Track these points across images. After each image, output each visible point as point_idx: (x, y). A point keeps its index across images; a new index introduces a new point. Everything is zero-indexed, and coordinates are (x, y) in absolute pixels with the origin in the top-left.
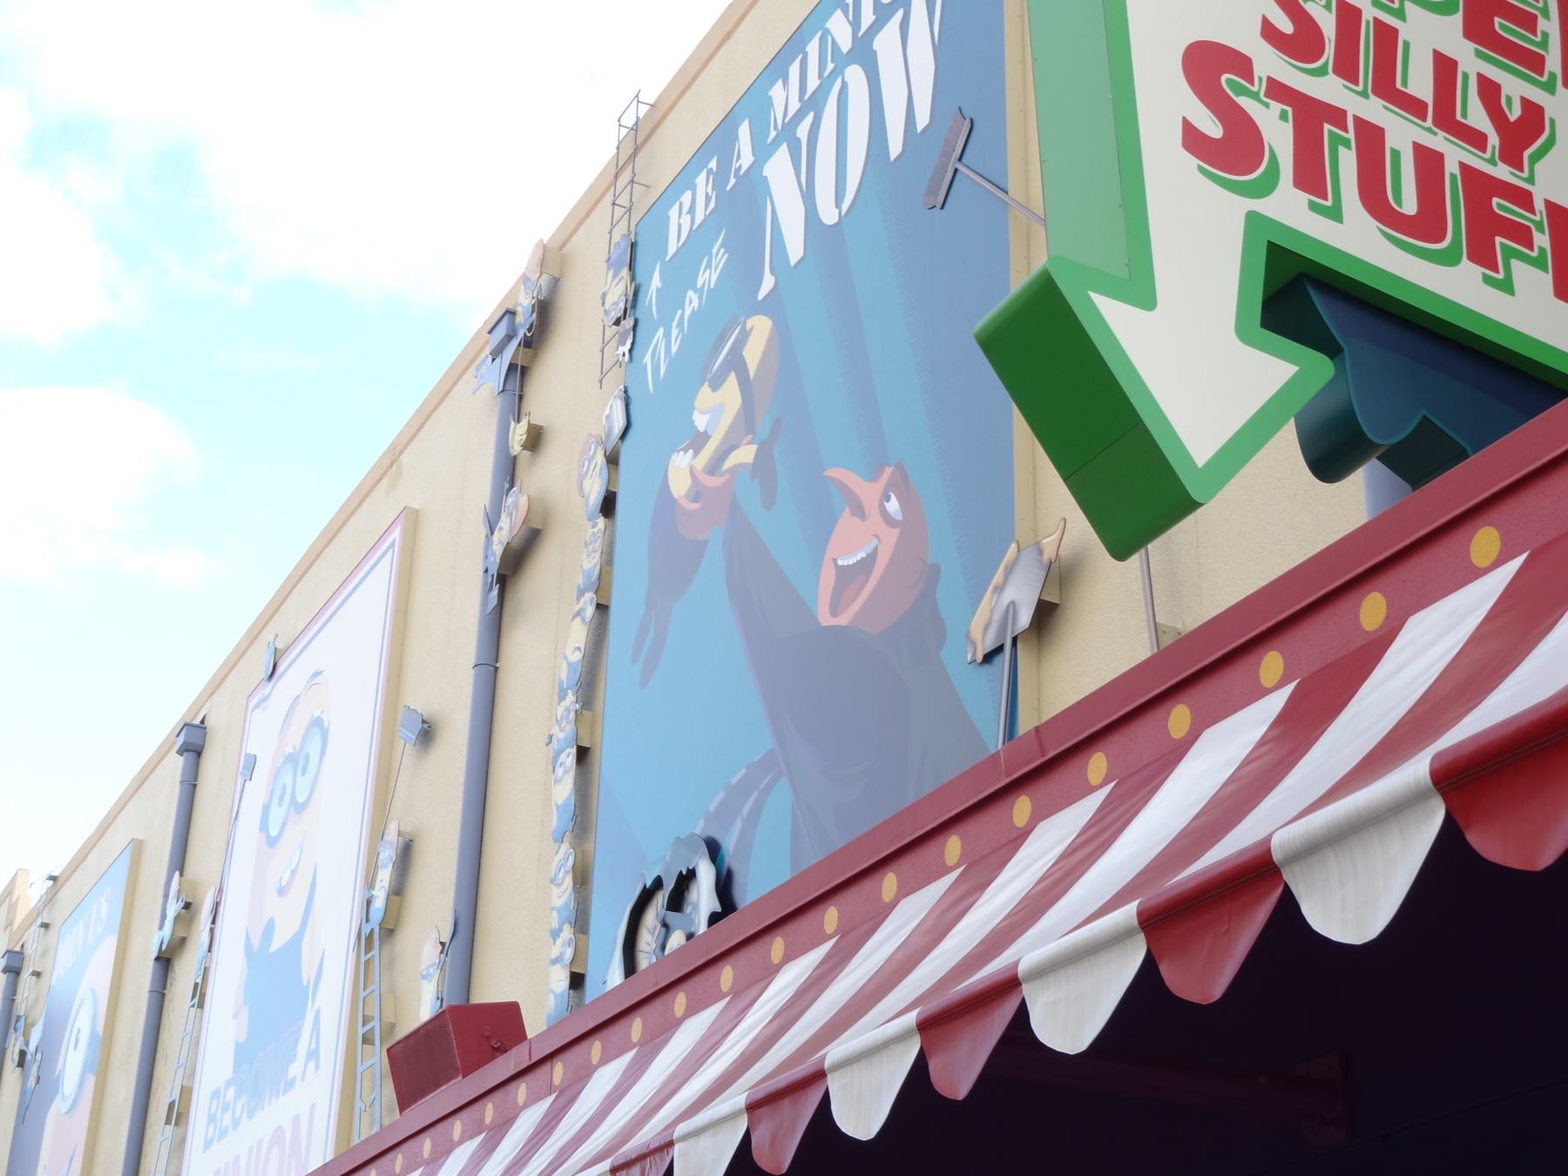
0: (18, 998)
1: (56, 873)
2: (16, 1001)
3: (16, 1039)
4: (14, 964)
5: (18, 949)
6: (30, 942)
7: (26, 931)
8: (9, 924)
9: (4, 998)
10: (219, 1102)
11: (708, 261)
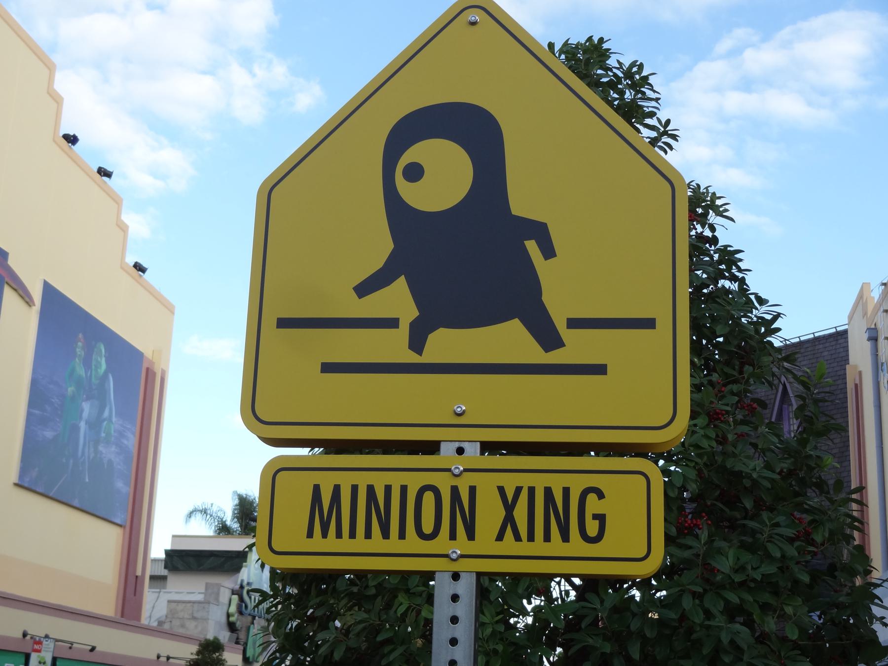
0: (880, 353)
1: (885, 281)
2: (879, 355)
3: (884, 376)
4: (874, 335)
5: (873, 326)
6: (879, 321)
7: (875, 316)
8: (865, 314)
9: (872, 354)
10: (319, 450)
11: (266, 646)
